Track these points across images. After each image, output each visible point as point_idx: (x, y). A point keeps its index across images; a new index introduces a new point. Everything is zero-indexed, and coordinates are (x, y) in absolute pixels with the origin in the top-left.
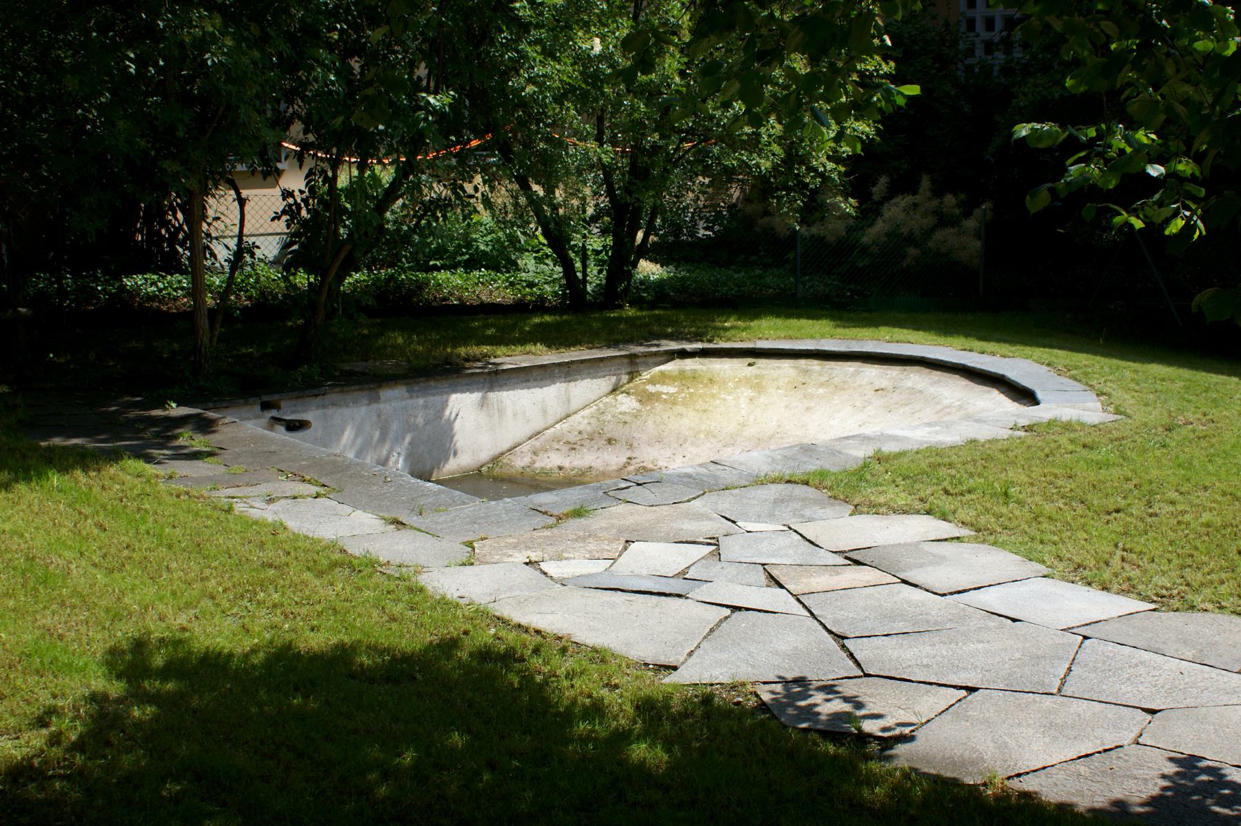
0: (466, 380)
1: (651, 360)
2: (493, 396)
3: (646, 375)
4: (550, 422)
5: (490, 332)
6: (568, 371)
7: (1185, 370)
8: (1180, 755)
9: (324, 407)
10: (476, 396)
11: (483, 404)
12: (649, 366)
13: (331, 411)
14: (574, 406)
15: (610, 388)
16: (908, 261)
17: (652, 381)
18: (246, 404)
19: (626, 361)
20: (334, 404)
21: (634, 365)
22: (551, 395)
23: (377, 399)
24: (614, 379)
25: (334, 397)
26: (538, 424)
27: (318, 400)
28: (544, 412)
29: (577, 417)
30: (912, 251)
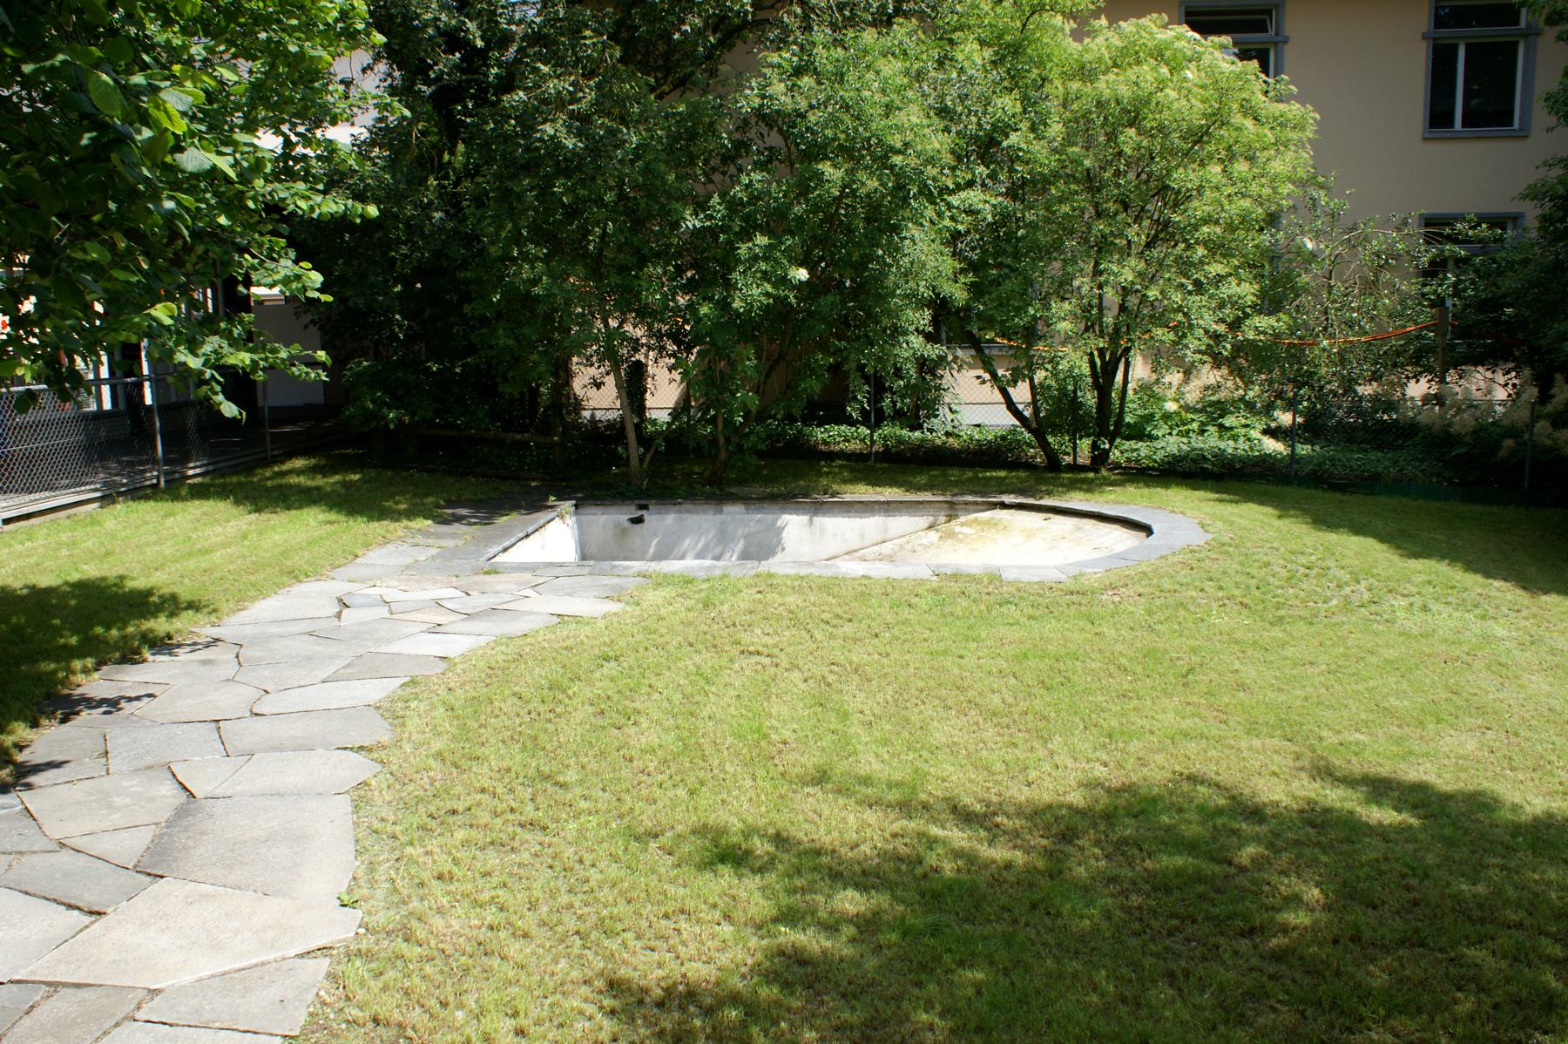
0: (793, 506)
1: (970, 507)
2: (818, 520)
3: (963, 519)
4: (867, 543)
5: (403, 507)
6: (888, 507)
7: (1251, 505)
8: (1077, 501)
9: (680, 512)
10: (804, 518)
11: (811, 521)
12: (968, 512)
13: (685, 516)
14: (889, 536)
15: (927, 525)
16: (1502, 454)
17: (962, 524)
18: (623, 504)
19: (945, 506)
20: (688, 512)
21: (952, 511)
22: (872, 524)
23: (721, 512)
24: (931, 519)
25: (688, 506)
26: (855, 544)
27: (677, 507)
28: (862, 536)
29: (889, 544)
30: (1509, 443)
